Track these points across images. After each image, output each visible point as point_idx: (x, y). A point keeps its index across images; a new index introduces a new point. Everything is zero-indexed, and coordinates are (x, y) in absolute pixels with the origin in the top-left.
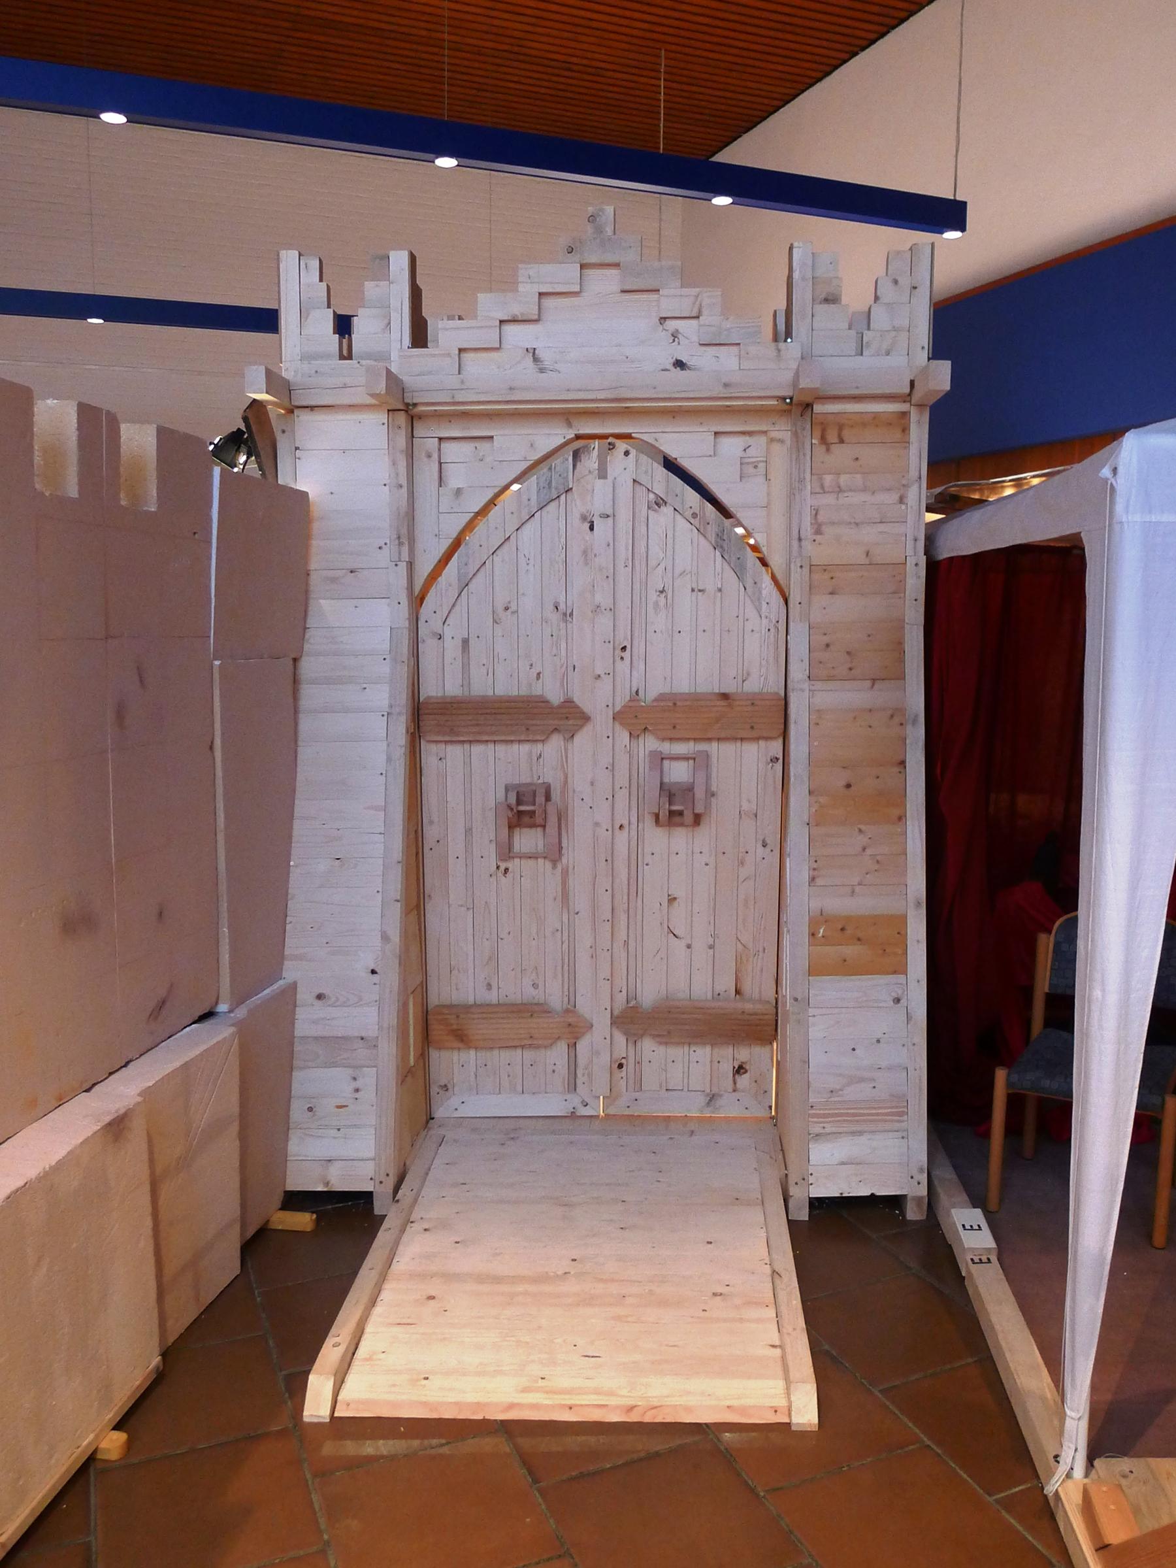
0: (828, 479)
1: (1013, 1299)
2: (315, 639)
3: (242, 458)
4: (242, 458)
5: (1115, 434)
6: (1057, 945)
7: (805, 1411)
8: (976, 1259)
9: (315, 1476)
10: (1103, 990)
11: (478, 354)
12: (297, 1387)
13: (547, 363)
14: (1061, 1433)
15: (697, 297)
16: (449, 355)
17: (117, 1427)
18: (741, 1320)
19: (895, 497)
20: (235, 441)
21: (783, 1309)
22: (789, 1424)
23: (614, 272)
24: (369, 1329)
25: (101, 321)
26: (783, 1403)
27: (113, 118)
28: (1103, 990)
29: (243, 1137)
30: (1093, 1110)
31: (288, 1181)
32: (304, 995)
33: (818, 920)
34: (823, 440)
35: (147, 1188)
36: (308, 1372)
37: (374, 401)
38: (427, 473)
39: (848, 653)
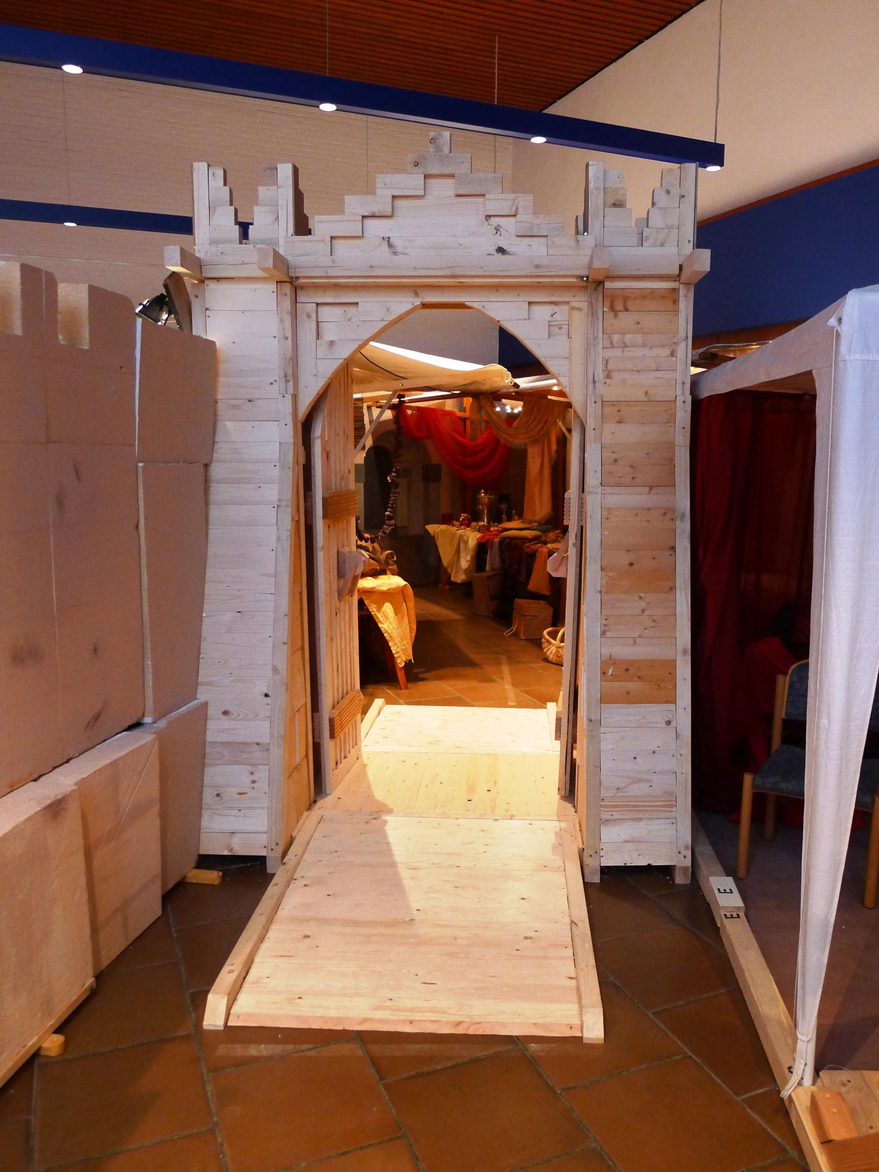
0: (616, 338)
1: (756, 945)
2: (222, 450)
3: (165, 316)
4: (165, 316)
5: (842, 293)
6: (791, 685)
7: (594, 1029)
8: (728, 915)
9: (209, 1071)
10: (829, 719)
11: (344, 241)
12: (199, 1003)
13: (399, 248)
14: (794, 1050)
15: (515, 200)
16: (323, 241)
17: (56, 1032)
18: (546, 958)
19: (667, 351)
20: (159, 303)
21: (579, 951)
22: (582, 1037)
23: (451, 181)
24: (257, 959)
25: (74, 225)
26: (576, 1021)
27: (72, 69)
28: (829, 719)
29: (163, 816)
30: (820, 809)
31: (201, 848)
32: (213, 711)
33: (608, 663)
34: (612, 308)
35: (81, 852)
36: (208, 992)
37: (266, 275)
38: (307, 329)
39: (632, 466)
